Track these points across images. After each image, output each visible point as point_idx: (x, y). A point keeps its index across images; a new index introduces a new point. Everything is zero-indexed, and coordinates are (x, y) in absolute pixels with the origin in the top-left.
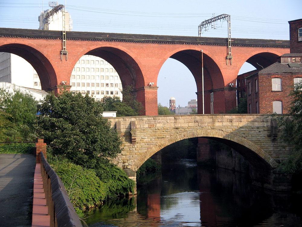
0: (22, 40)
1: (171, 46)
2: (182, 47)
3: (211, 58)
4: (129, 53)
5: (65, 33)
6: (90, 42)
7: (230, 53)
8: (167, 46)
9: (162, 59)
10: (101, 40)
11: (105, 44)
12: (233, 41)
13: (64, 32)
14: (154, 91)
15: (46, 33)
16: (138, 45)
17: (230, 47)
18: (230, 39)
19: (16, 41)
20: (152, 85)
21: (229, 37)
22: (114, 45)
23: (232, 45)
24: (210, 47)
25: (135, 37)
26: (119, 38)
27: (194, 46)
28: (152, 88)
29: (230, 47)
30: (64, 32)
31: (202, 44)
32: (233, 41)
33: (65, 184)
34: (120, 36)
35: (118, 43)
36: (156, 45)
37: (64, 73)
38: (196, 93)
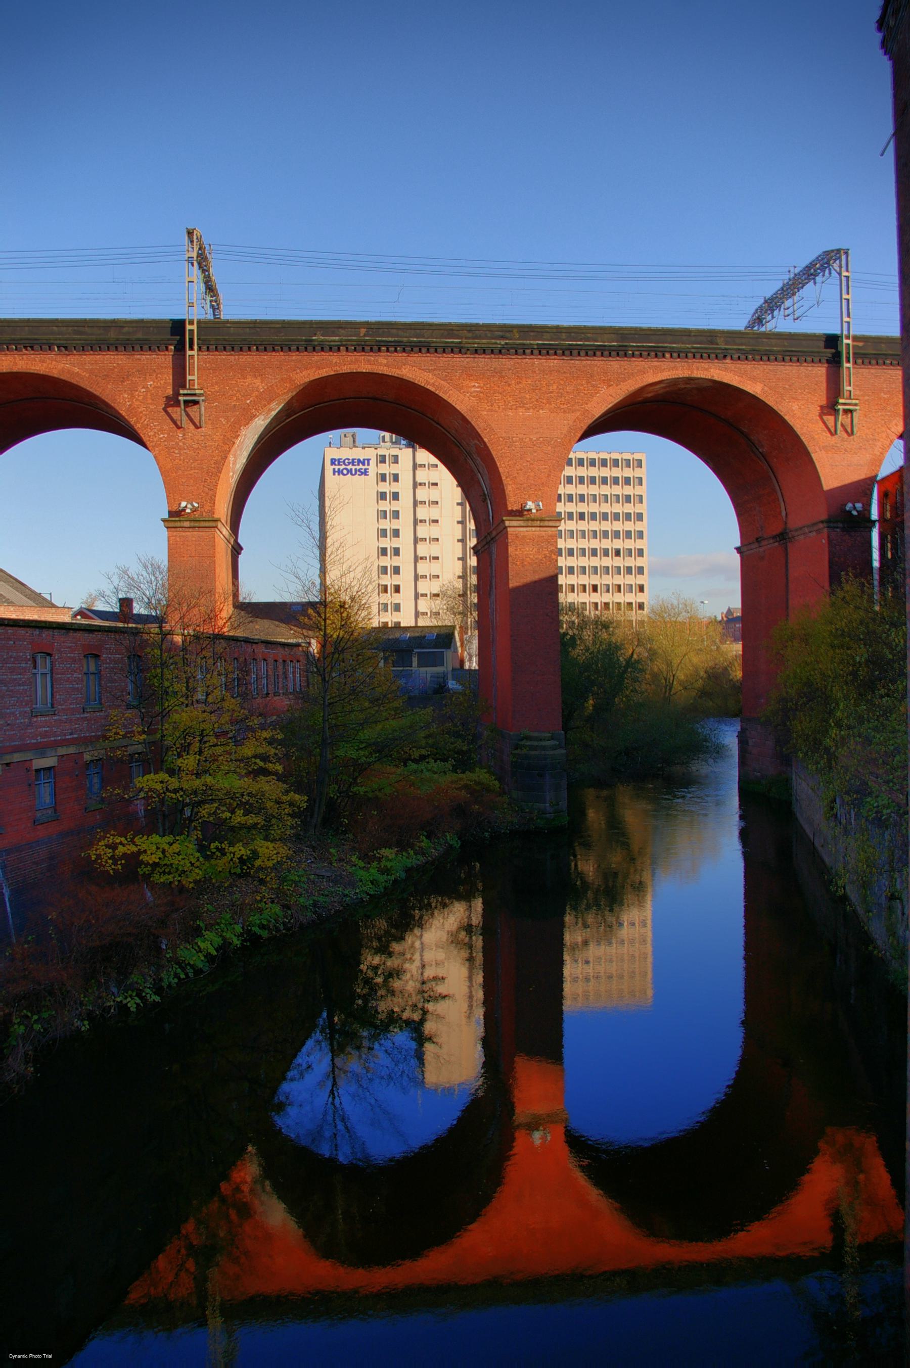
0: (38, 358)
1: (615, 365)
2: (656, 367)
3: (775, 408)
4: (445, 393)
5: (195, 327)
6: (295, 356)
7: (848, 388)
8: (597, 364)
9: (578, 413)
10: (332, 348)
11: (352, 363)
12: (861, 344)
13: (191, 322)
14: (543, 534)
15: (125, 330)
16: (482, 362)
17: (850, 365)
18: (848, 338)
19: (15, 364)
20: (534, 511)
21: (845, 332)
22: (387, 365)
23: (855, 363)
24: (771, 368)
25: (470, 335)
26: (405, 339)
27: (706, 366)
28: (538, 523)
29: (850, 365)
30: (191, 322)
31: (735, 356)
32: (861, 344)
33: (265, 902)
34: (413, 332)
35: (401, 357)
36: (554, 362)
37: (191, 472)
38: (738, 549)
